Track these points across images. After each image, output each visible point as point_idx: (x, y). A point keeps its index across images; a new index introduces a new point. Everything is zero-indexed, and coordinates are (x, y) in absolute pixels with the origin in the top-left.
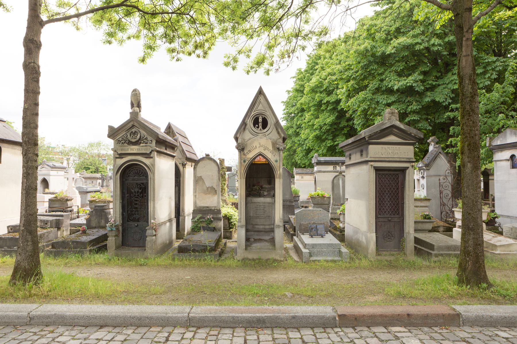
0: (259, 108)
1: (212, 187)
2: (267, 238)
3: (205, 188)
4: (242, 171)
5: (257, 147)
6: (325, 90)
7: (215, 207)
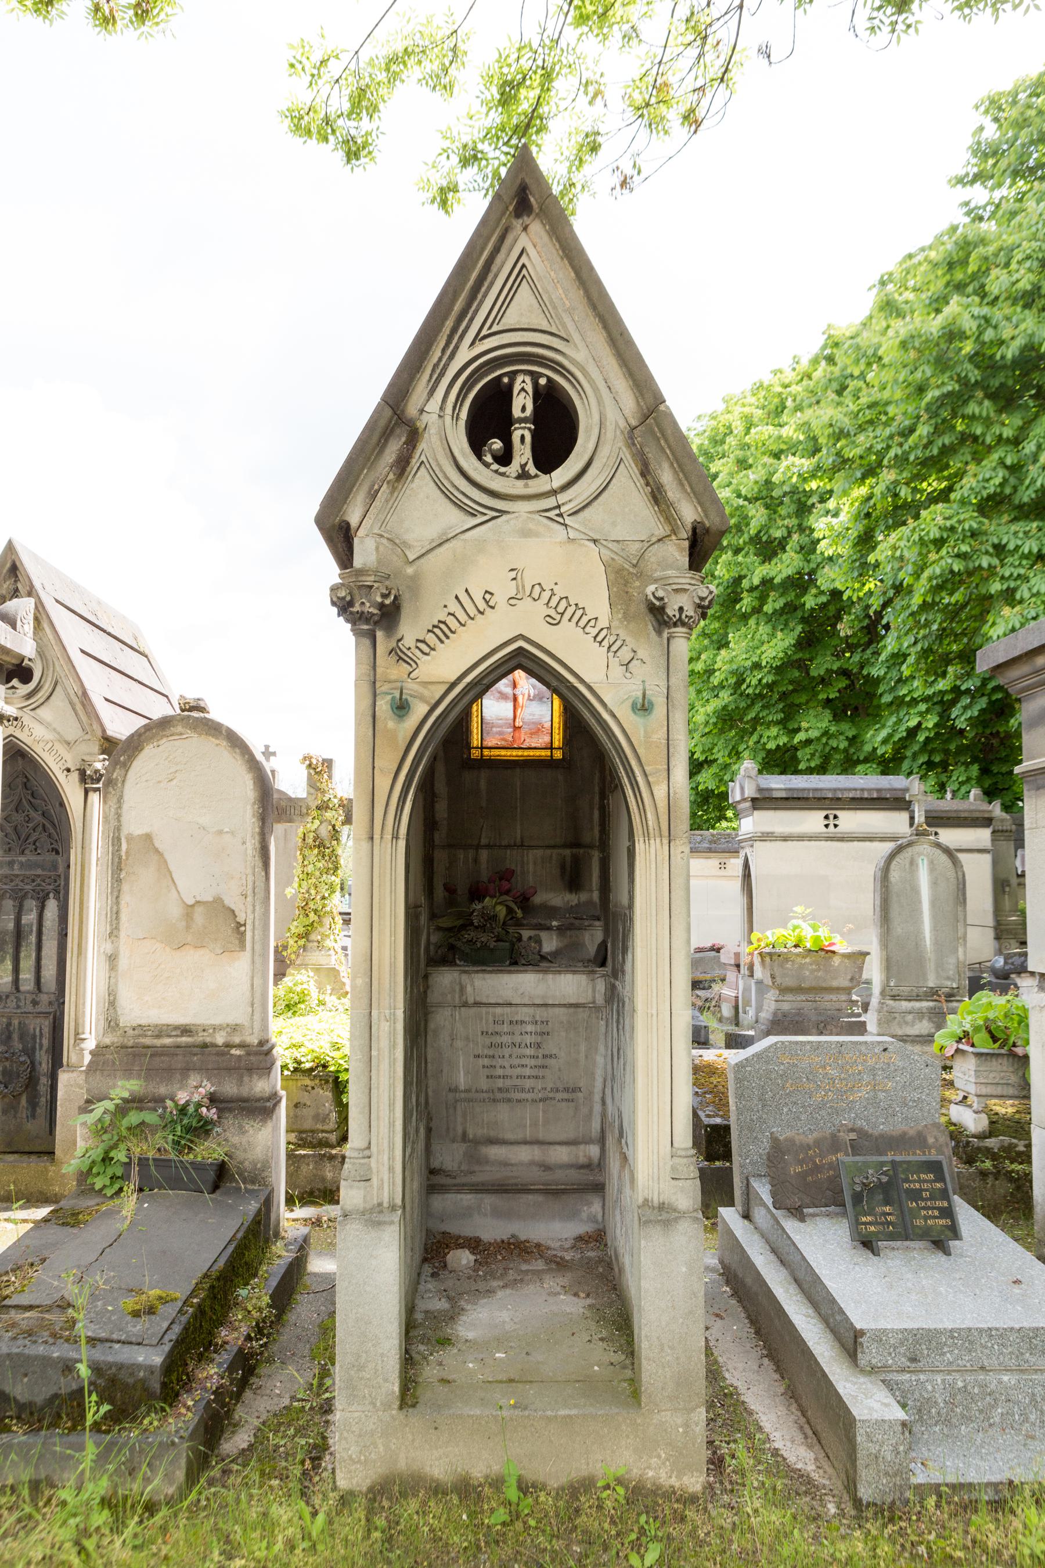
0: (511, 319)
1: (218, 901)
2: (556, 1231)
3: (175, 911)
4: (383, 783)
5: (500, 599)
6: (755, 540)
7: (235, 1028)
